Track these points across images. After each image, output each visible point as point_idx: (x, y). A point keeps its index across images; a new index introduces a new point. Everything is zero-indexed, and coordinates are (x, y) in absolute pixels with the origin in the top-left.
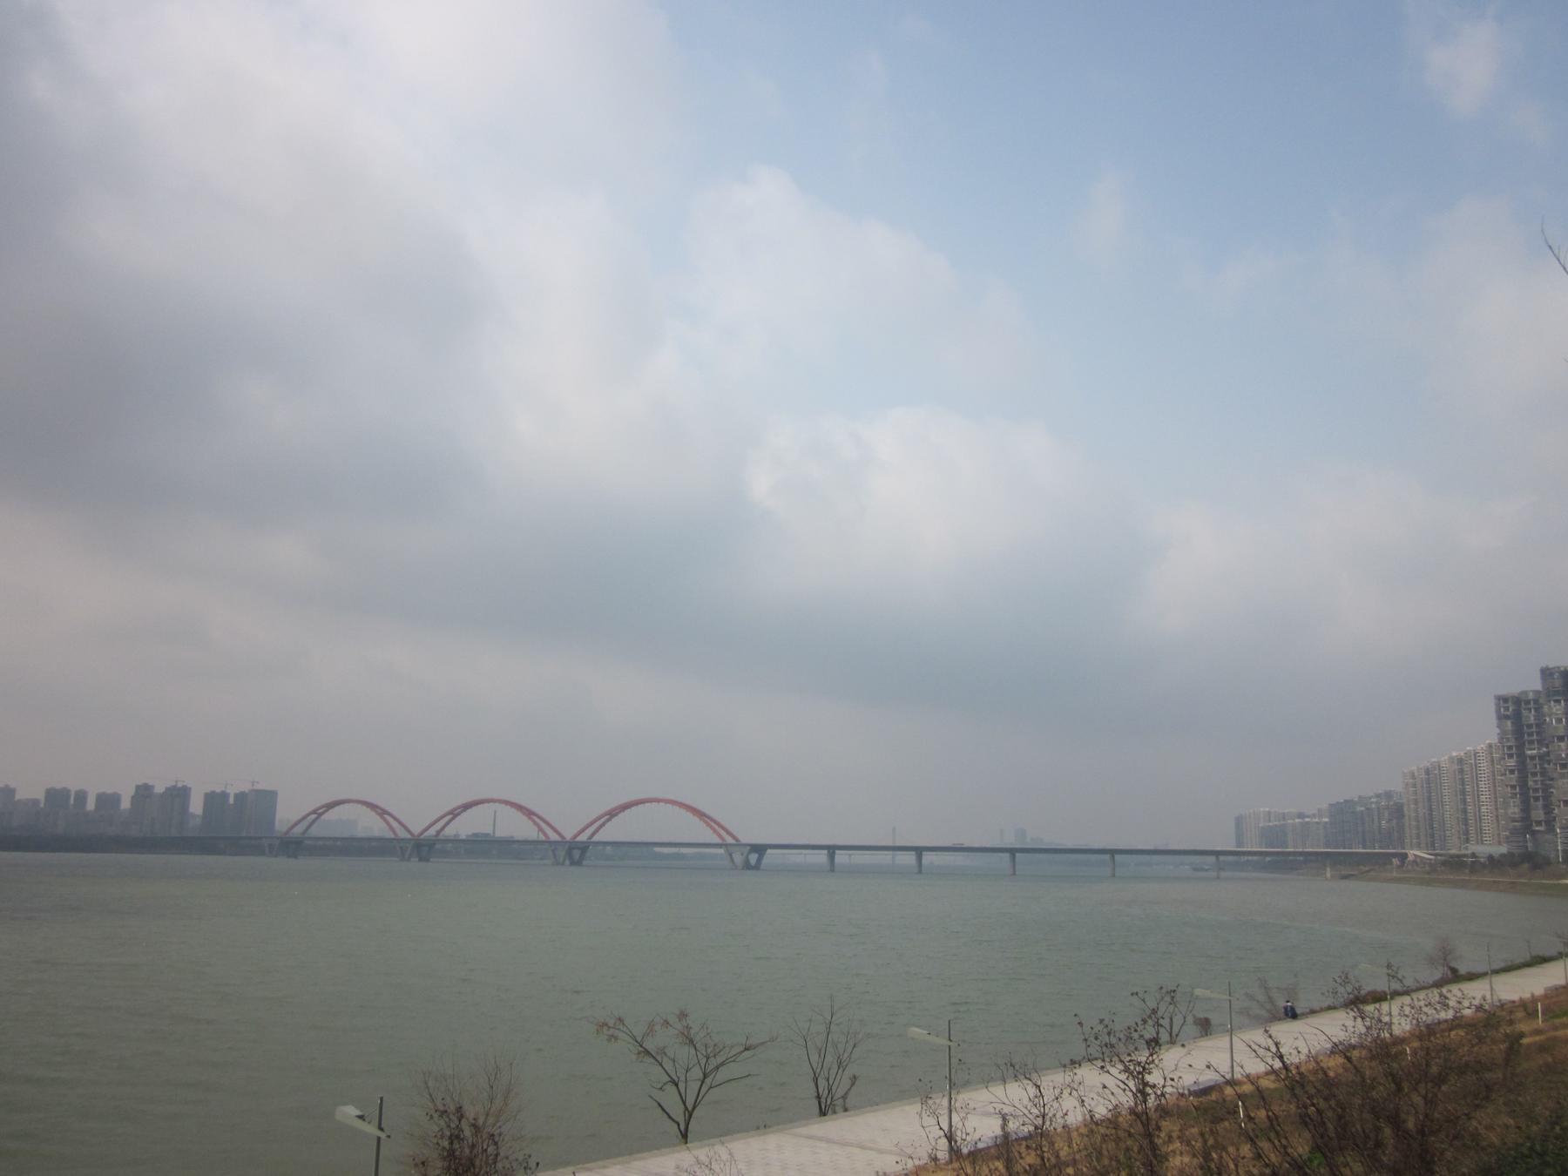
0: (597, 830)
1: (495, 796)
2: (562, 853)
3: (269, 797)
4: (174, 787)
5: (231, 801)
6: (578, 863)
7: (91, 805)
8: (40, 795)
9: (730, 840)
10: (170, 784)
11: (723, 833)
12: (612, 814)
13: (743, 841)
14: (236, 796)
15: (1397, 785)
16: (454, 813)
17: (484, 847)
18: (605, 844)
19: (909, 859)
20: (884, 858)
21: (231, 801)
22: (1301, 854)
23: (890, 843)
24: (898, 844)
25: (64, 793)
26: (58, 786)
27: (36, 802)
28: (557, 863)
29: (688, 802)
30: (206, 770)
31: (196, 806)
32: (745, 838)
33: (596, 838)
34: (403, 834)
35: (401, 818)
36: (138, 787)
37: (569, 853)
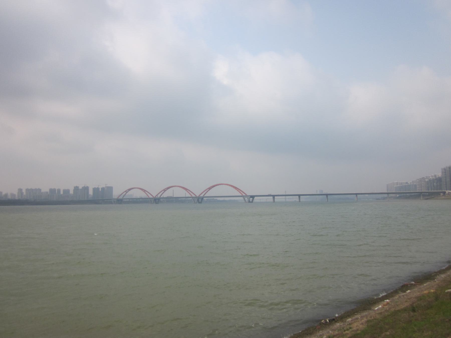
0: (205, 194)
2: (196, 200)
3: (110, 189)
4: (84, 187)
5: (100, 190)
6: (201, 203)
7: (62, 193)
8: (48, 191)
9: (244, 195)
10: (83, 186)
12: (210, 189)
13: (248, 195)
14: (102, 188)
15: (439, 174)
16: (165, 190)
20: (289, 199)
21: (100, 190)
22: (427, 192)
23: (284, 194)
24: (287, 194)
25: (54, 190)
27: (47, 192)
30: (93, 182)
31: (91, 192)
34: (151, 197)
35: (151, 194)
36: (75, 187)
37: (198, 200)
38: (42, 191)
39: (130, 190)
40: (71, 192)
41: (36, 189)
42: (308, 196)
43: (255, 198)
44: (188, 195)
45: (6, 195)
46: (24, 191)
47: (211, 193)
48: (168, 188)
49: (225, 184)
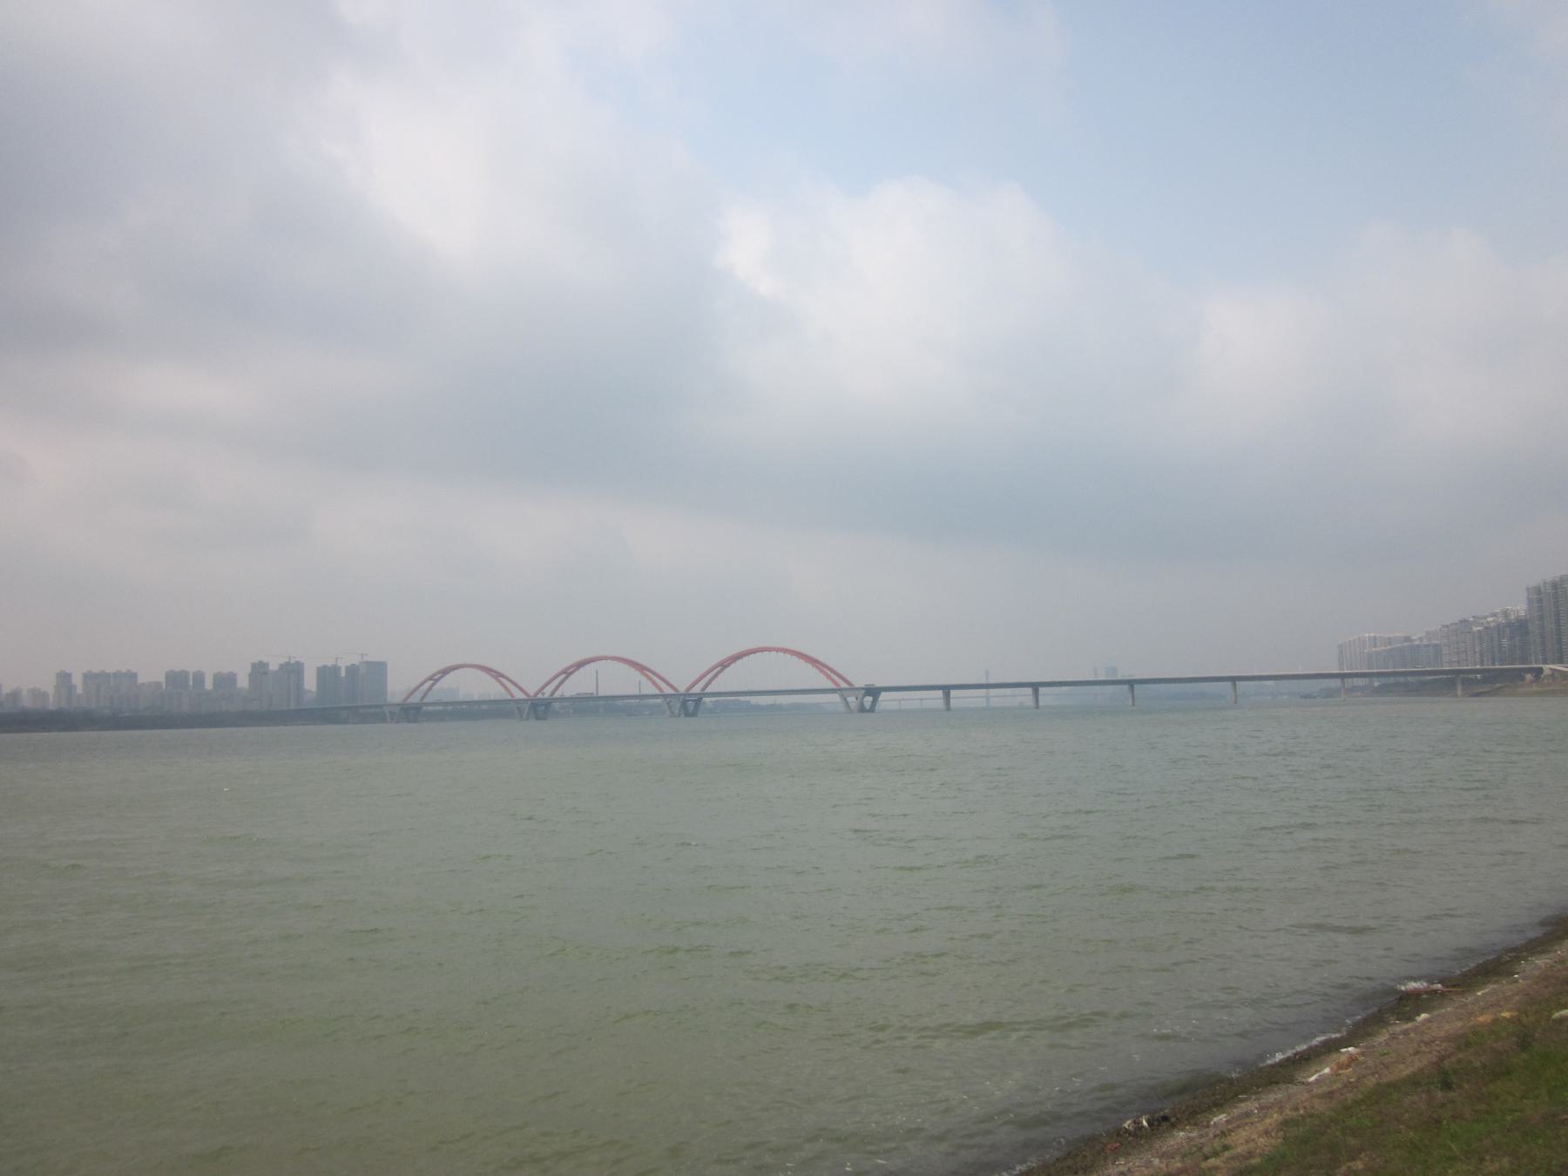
1: (469, 662)
4: (288, 664)
5: (343, 674)
6: (694, 714)
7: (209, 685)
8: (162, 679)
9: (843, 685)
11: (663, 685)
12: (723, 665)
13: (857, 685)
14: (347, 668)
16: (568, 672)
17: (587, 706)
18: (435, 704)
20: (998, 698)
21: (343, 674)
23: (983, 681)
24: (992, 681)
25: (183, 675)
26: (177, 668)
27: (158, 684)
28: (672, 714)
30: (317, 646)
31: (310, 683)
32: (860, 682)
33: (708, 690)
34: (519, 695)
36: (253, 665)
37: (684, 705)
38: (141, 679)
39: (445, 672)
40: (243, 682)
41: (118, 675)
43: (884, 695)
44: (649, 689)
46: (77, 681)
47: (728, 681)
48: (606, 658)
49: (778, 650)
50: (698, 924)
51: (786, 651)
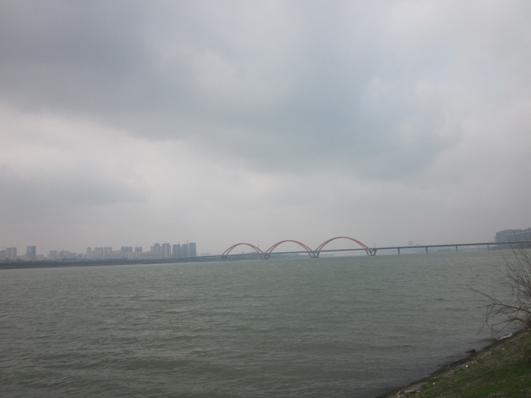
9: (309, 250)
12: (276, 245)
13: (369, 247)
16: (232, 248)
18: (275, 253)
19: (395, 252)
26: (125, 246)
29: (356, 239)
33: (272, 252)
37: (265, 257)
38: (113, 250)
41: (106, 248)
42: (392, 250)
45: (80, 255)
46: (93, 249)
47: (276, 250)
48: (284, 241)
50: (456, 324)
51: (293, 241)
